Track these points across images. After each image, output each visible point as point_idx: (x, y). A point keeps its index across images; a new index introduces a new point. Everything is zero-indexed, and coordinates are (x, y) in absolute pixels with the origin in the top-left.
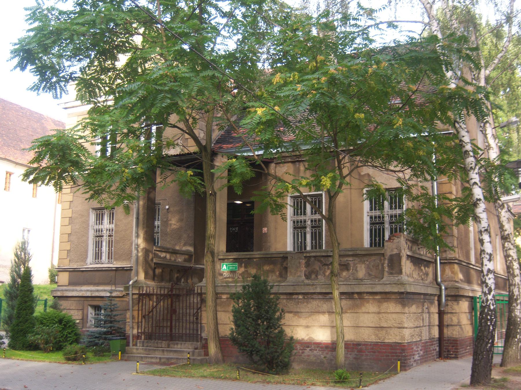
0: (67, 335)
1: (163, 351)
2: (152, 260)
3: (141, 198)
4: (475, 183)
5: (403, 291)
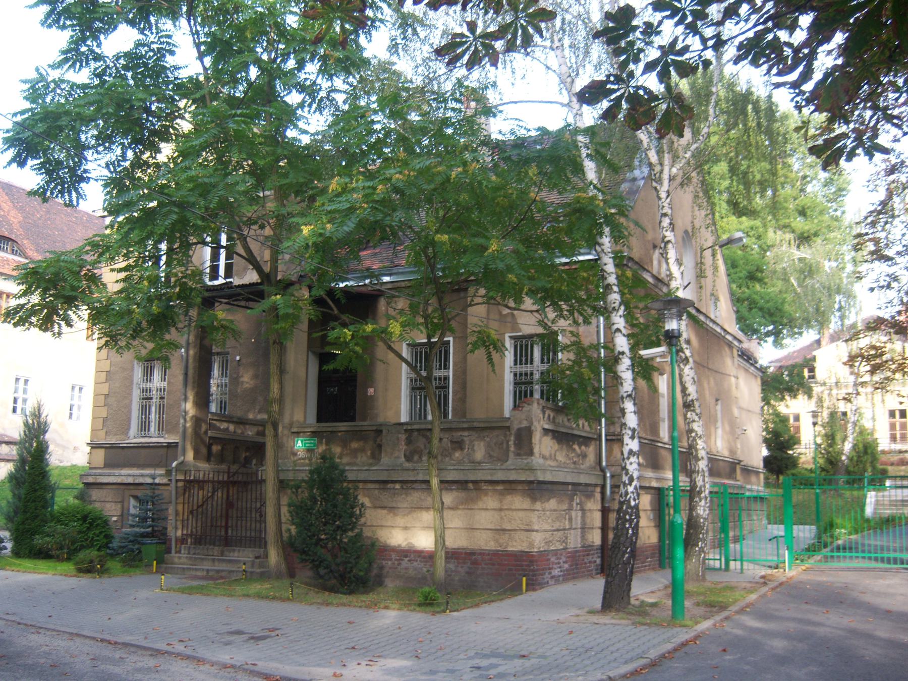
0: (93, 538)
1: (213, 560)
2: (206, 433)
3: (191, 346)
4: (618, 330)
5: (532, 479)
